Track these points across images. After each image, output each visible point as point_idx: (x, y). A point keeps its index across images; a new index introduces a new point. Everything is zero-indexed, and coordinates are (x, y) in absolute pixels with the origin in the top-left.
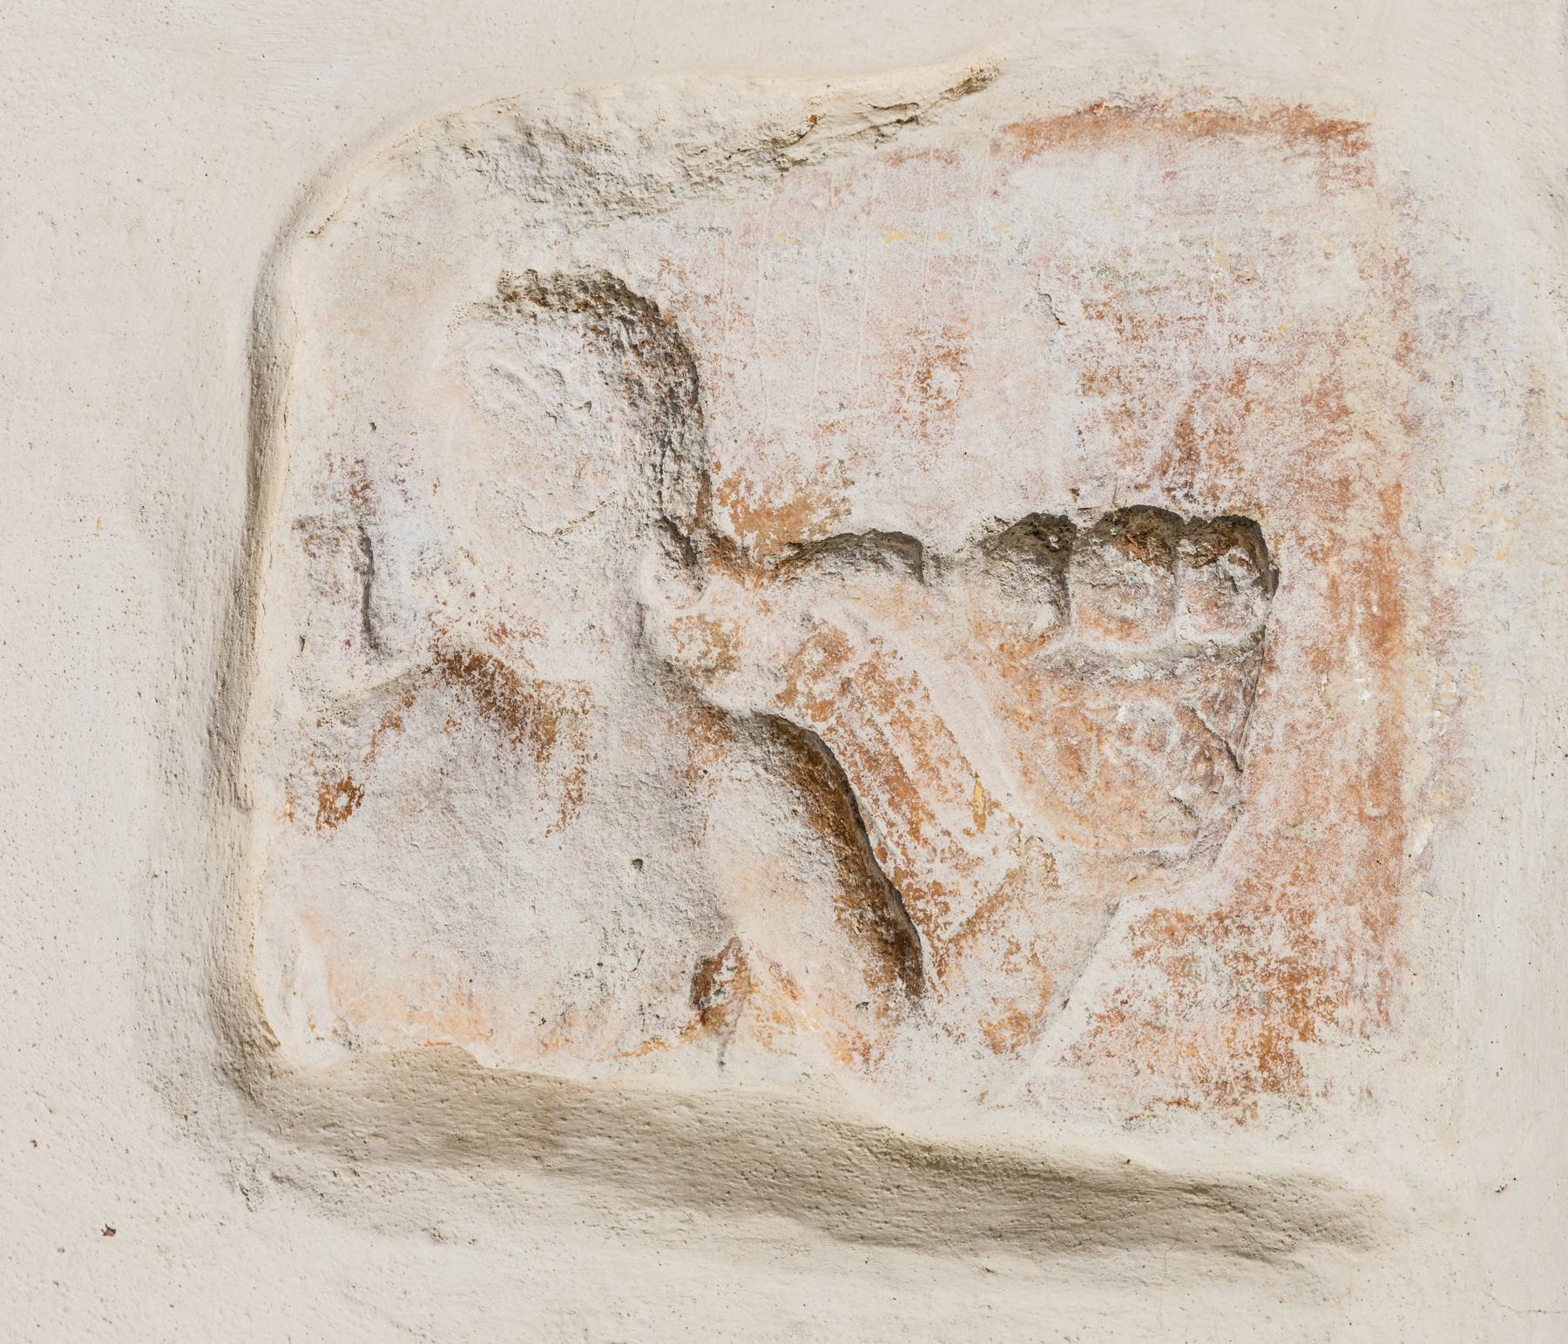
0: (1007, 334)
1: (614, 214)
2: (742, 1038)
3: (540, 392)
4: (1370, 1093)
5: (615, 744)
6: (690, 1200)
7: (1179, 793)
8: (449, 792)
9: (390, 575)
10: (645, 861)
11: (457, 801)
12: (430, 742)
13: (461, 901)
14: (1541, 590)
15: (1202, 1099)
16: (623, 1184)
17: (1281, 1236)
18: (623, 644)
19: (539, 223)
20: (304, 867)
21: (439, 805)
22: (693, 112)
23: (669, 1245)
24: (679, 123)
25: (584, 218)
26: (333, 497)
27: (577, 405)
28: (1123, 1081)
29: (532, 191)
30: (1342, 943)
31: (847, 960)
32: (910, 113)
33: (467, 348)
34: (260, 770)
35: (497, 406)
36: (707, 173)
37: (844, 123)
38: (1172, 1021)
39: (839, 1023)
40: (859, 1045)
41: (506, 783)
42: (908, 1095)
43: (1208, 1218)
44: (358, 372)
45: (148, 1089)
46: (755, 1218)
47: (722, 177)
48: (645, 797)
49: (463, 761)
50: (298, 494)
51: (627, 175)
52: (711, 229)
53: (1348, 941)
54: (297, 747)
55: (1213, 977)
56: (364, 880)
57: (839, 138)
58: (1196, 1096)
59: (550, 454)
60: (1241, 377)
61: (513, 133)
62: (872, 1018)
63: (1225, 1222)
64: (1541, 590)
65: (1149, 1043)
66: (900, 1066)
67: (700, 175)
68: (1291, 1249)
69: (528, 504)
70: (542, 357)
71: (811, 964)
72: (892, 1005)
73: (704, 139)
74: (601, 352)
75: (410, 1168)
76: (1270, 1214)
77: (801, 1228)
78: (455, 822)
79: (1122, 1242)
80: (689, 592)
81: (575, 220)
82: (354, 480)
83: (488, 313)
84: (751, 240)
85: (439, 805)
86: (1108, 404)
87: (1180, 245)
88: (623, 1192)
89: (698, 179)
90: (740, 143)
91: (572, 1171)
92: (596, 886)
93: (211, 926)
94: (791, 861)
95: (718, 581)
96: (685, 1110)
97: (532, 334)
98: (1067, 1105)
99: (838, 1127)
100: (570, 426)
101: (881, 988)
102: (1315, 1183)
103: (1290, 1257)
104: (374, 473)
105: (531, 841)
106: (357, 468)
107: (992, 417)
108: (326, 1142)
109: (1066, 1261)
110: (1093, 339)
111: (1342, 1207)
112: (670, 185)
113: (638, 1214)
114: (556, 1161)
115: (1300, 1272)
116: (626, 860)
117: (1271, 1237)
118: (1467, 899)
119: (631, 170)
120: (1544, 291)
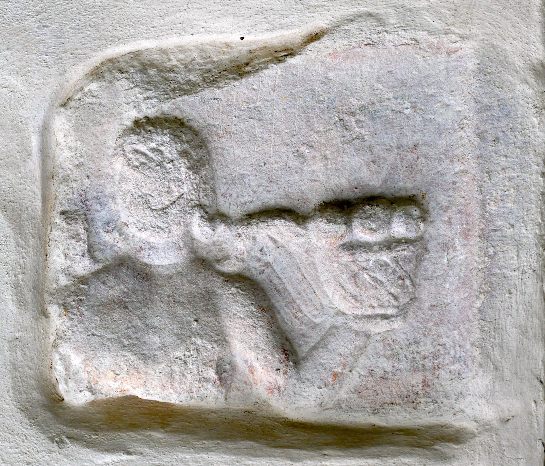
0: (327, 134)
1: (177, 95)
2: (233, 391)
3: (154, 158)
4: (461, 393)
5: (186, 284)
6: (218, 438)
7: (392, 290)
8: (126, 302)
9: (96, 233)
10: (199, 320)
11: (128, 305)
12: (117, 288)
13: (133, 336)
14: (526, 213)
15: (401, 402)
16: (193, 434)
17: (429, 442)
18: (186, 250)
19: (149, 98)
20: (73, 332)
21: (122, 307)
22: (205, 57)
23: (212, 451)
24: (200, 61)
25: (166, 96)
26: (74, 204)
27: (168, 161)
28: (372, 397)
29: (146, 86)
30: (452, 344)
31: (273, 356)
32: (290, 52)
33: (124, 145)
34: (51, 302)
35: (137, 164)
36: (212, 79)
37: (264, 58)
38: (390, 376)
39: (269, 378)
40: (276, 386)
41: (146, 299)
42: (295, 403)
43: (405, 438)
44: (82, 156)
45: (19, 410)
46: (242, 442)
47: (218, 80)
48: (198, 300)
49: (130, 293)
50: (61, 203)
51: (181, 81)
52: (214, 99)
53: (454, 343)
54: (66, 294)
55: (405, 359)
56: (96, 332)
57: (263, 63)
58: (399, 401)
59: (159, 180)
60: (416, 146)
61: (138, 65)
62: (282, 375)
63: (409, 439)
64: (526, 213)
65: (381, 384)
66: (292, 393)
67: (209, 79)
68: (433, 445)
69: (150, 199)
70: (153, 145)
71: (259, 357)
72: (288, 370)
73: (210, 66)
74: (176, 143)
75: (116, 433)
76: (425, 436)
77: (258, 445)
78: (128, 311)
79: (372, 445)
80: (210, 231)
81: (162, 97)
82: (81, 198)
83: (131, 132)
84: (230, 103)
85: (122, 307)
86: (365, 158)
87: (393, 99)
88: (194, 436)
89: (209, 81)
90: (225, 68)
91: (174, 432)
92: (182, 328)
93: (37, 357)
94: (251, 320)
95: (221, 228)
96: (214, 414)
97: (150, 137)
98: (352, 407)
99: (269, 418)
100: (166, 170)
101: (284, 364)
102: (442, 427)
103: (433, 447)
104: (89, 196)
105: (157, 316)
106: (83, 193)
107: (322, 165)
108: (85, 427)
109: (352, 451)
110: (360, 135)
111: (452, 433)
112: (198, 83)
113: (200, 443)
114: (169, 429)
115: (436, 451)
116: (192, 320)
117: (425, 442)
118: (497, 321)
119: (183, 79)
120: (531, 106)
